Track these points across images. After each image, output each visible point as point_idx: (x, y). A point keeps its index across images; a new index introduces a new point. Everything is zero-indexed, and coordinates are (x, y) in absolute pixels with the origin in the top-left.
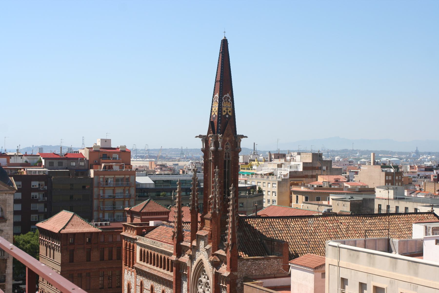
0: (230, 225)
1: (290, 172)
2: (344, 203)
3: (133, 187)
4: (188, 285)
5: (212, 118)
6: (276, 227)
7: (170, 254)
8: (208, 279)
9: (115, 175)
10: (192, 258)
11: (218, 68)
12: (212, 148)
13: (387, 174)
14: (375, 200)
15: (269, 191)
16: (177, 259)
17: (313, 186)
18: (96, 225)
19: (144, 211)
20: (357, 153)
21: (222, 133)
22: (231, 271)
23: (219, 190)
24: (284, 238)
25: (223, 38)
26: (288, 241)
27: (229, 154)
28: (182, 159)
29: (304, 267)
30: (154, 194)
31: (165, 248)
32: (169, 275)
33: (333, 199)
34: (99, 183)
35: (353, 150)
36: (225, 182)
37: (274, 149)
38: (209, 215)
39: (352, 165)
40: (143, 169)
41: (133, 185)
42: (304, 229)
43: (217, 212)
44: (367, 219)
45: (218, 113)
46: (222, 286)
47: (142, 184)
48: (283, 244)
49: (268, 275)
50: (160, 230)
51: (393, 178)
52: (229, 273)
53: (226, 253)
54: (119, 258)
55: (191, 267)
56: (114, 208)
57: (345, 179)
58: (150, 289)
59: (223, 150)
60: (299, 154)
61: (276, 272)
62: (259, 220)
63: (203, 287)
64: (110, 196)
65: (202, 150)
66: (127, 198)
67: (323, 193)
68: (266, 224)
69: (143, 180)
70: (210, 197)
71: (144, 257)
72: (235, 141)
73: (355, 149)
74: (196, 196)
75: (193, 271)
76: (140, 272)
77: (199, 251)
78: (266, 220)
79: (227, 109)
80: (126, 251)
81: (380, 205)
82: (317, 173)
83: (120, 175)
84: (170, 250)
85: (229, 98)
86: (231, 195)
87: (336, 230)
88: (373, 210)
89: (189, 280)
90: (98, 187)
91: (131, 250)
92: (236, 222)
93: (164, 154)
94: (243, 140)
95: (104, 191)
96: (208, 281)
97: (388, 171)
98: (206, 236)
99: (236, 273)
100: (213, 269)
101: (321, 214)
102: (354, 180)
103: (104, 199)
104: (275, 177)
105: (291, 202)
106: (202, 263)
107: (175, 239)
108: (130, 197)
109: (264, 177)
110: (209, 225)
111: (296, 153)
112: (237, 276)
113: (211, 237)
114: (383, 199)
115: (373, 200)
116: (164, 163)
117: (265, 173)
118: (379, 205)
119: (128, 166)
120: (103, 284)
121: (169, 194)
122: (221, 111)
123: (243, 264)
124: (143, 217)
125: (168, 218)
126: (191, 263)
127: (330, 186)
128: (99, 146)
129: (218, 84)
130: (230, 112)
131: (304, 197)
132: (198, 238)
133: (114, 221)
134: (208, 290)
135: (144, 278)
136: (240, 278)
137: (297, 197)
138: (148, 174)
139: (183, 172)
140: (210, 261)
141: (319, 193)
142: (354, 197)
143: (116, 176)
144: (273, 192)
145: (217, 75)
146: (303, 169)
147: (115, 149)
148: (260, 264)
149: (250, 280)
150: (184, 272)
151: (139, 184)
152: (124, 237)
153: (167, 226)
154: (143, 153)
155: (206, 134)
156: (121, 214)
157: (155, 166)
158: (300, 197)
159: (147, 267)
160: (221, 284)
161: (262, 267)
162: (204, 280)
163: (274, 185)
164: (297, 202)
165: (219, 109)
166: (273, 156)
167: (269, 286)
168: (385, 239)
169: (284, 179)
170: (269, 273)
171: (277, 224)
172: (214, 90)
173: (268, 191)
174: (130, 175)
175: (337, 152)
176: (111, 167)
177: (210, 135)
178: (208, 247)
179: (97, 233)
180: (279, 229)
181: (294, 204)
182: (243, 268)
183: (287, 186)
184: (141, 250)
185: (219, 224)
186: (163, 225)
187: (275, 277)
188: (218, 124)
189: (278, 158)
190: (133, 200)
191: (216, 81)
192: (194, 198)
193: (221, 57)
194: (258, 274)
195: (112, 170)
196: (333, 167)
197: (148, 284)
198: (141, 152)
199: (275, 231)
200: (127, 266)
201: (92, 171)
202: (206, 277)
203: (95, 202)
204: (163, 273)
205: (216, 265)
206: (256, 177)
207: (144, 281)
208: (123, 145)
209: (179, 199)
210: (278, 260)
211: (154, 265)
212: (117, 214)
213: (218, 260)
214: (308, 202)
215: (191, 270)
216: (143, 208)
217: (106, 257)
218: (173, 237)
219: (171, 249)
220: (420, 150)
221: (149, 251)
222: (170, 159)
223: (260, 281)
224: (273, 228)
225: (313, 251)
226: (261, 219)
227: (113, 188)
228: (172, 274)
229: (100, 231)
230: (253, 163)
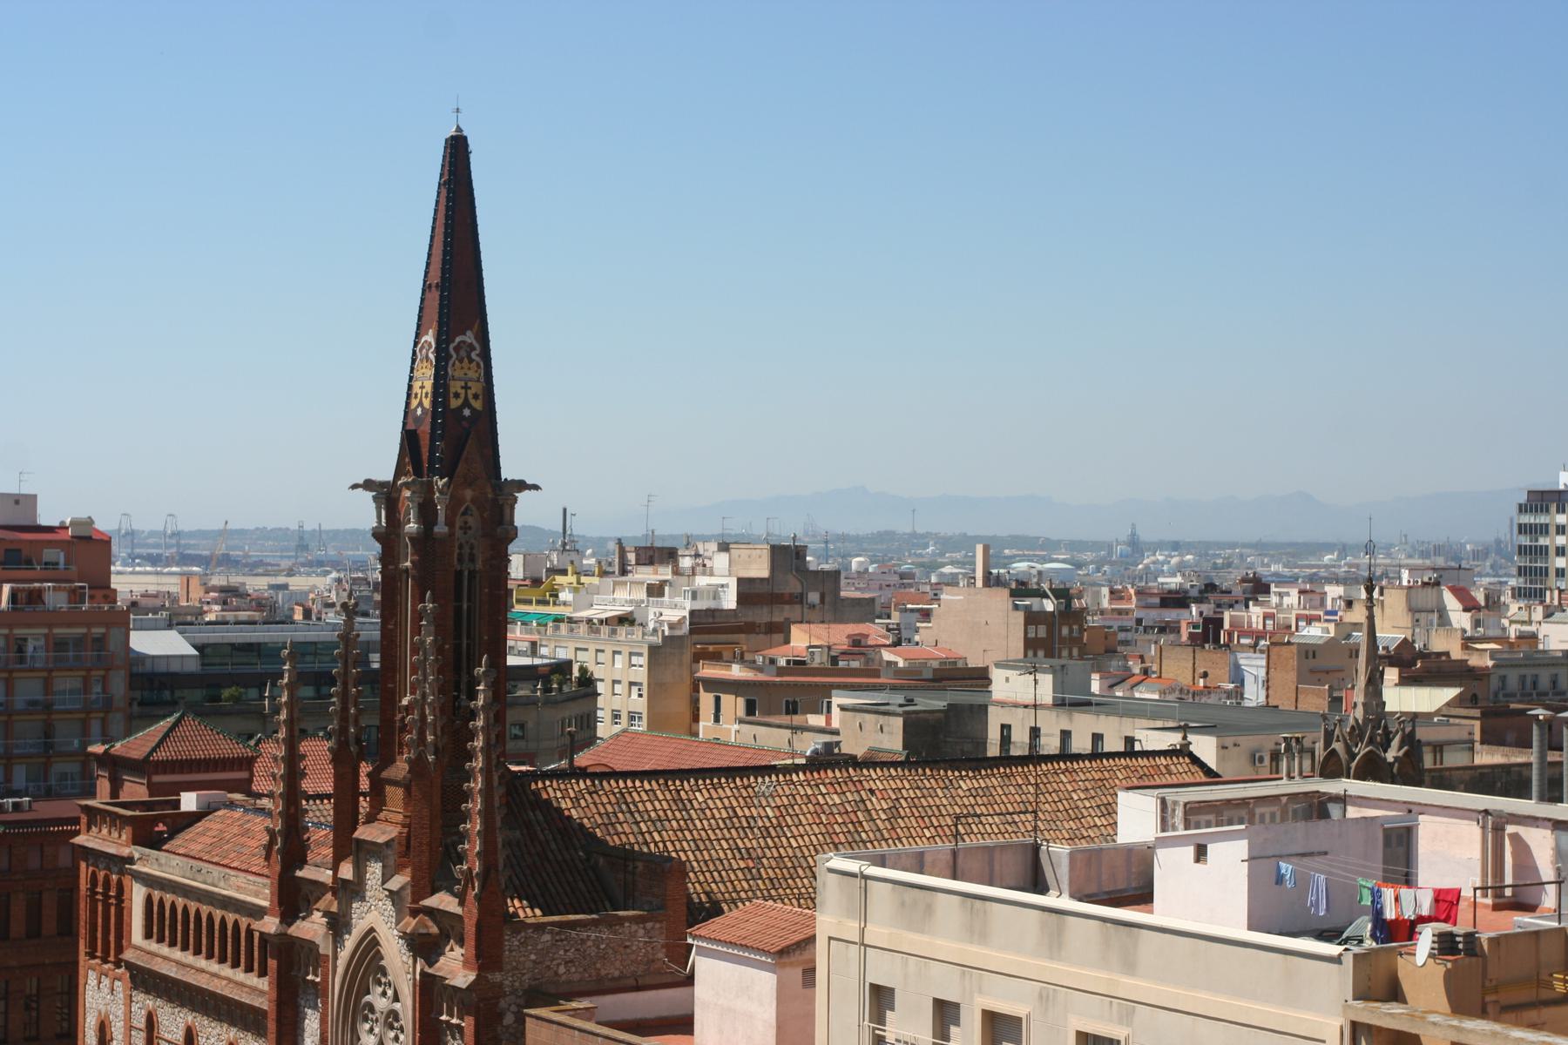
0: (476, 805)
1: (692, 613)
2: (882, 719)
4: (323, 1021)
5: (410, 420)
6: (641, 808)
7: (257, 912)
8: (396, 999)
12: (412, 526)
13: (1032, 618)
14: (991, 709)
15: (619, 682)
17: (772, 661)
19: (161, 755)
20: (926, 546)
21: (448, 472)
24: (671, 848)
25: (452, 132)
26: (684, 858)
27: (472, 548)
28: (303, 565)
29: (742, 949)
30: (197, 695)
31: (238, 889)
32: (255, 988)
33: (843, 708)
35: (914, 535)
36: (457, 649)
38: (400, 768)
39: (910, 586)
40: (158, 602)
42: (740, 813)
43: (431, 758)
45: (434, 403)
46: (447, 1022)
47: (154, 657)
48: (667, 870)
49: (614, 979)
51: (1050, 632)
52: (472, 977)
53: (462, 903)
55: (336, 958)
56: (48, 746)
59: (451, 534)
60: (724, 547)
61: (642, 968)
62: (582, 786)
63: (377, 1030)
64: (33, 703)
65: (377, 535)
67: (810, 685)
68: (605, 800)
70: (405, 702)
71: (160, 924)
72: (495, 500)
73: (920, 530)
74: (351, 701)
75: (340, 970)
76: (145, 980)
77: (363, 899)
78: (605, 783)
80: (94, 902)
81: (1006, 729)
83: (69, 625)
84: (257, 896)
88: (982, 743)
89: (325, 1003)
91: (113, 901)
94: (523, 497)
96: (397, 1006)
97: (1035, 608)
98: (388, 844)
99: (497, 977)
100: (415, 962)
101: (803, 761)
102: (917, 638)
103: (10, 715)
104: (638, 631)
105: (696, 718)
106: (375, 943)
107: (276, 858)
108: (108, 705)
109: (598, 631)
110: (401, 803)
111: (713, 546)
112: (501, 985)
113: (408, 847)
114: (1016, 705)
116: (235, 580)
117: (604, 616)
118: (1003, 726)
119: (99, 594)
122: (446, 396)
123: (523, 944)
124: (157, 779)
125: (250, 781)
127: (834, 660)
129: (435, 295)
130: (476, 397)
131: (741, 702)
133: (49, 794)
135: (159, 1002)
137: (718, 699)
138: (177, 619)
139: (307, 614)
140: (404, 936)
141: (795, 684)
142: (917, 700)
143: (56, 631)
144: (631, 684)
145: (428, 264)
146: (738, 602)
147: (50, 529)
148: (583, 941)
149: (550, 999)
150: (310, 977)
151: (142, 658)
154: (157, 546)
155: (388, 475)
157: (202, 594)
158: (727, 700)
159: (171, 960)
160: (444, 1018)
161: (593, 951)
162: (381, 1004)
163: (635, 660)
164: (717, 720)
165: (436, 386)
166: (632, 557)
168: (1024, 845)
170: (617, 973)
173: (615, 682)
174: (107, 625)
175: (857, 539)
176: (35, 597)
178: (397, 882)
181: (705, 725)
184: (149, 901)
186: (232, 805)
187: (638, 988)
188: (433, 439)
189: (651, 563)
191: (426, 288)
192: (345, 709)
194: (576, 977)
195: (40, 608)
196: (843, 594)
198: (150, 541)
199: (637, 823)
200: (94, 957)
202: (390, 992)
204: (230, 980)
205: (424, 947)
206: (572, 630)
207: (159, 1011)
208: (82, 514)
210: (649, 925)
211: (197, 952)
212: (58, 767)
213: (434, 930)
214: (757, 717)
216: (158, 746)
218: (269, 848)
219: (258, 891)
220: (1145, 535)
221: (180, 902)
222: (254, 567)
225: (773, 892)
226: (589, 782)
227: (45, 674)
228: (263, 984)
230: (559, 579)
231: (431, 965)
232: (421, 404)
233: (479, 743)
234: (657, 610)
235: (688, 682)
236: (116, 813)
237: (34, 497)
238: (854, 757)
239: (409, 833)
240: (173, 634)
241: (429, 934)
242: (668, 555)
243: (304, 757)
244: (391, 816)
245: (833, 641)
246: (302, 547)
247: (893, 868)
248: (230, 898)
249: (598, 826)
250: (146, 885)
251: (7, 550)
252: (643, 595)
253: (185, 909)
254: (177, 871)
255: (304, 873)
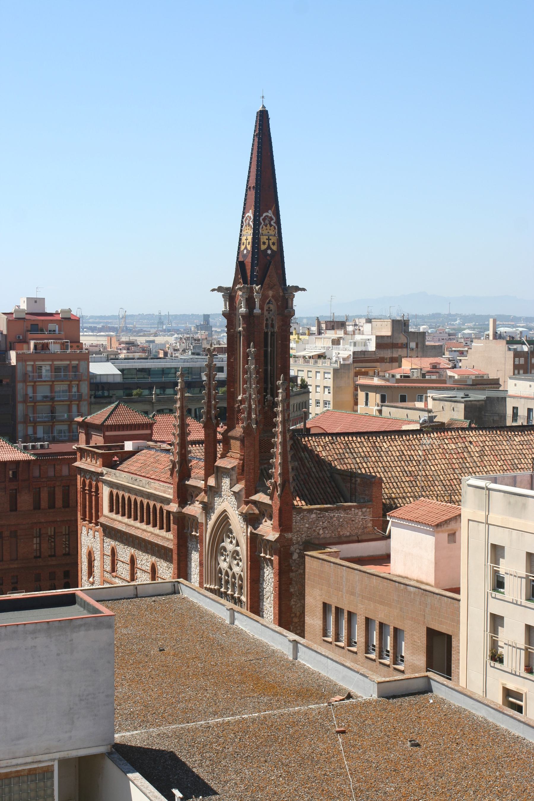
0: (278, 450)
1: (354, 353)
2: (453, 404)
3: (85, 380)
4: (201, 556)
5: (240, 256)
6: (357, 451)
7: (167, 501)
8: (238, 545)
9: (53, 360)
10: (208, 508)
11: (251, 163)
12: (243, 310)
13: (517, 354)
14: (508, 399)
15: (319, 386)
16: (180, 509)
17: (393, 376)
18: (25, 448)
20: (456, 320)
21: (261, 282)
22: (281, 531)
23: (257, 387)
24: (372, 471)
25: (260, 108)
26: (379, 476)
27: (272, 320)
28: (161, 331)
29: (416, 524)
30: (120, 393)
31: (155, 489)
32: (166, 538)
33: (434, 399)
34: (25, 374)
35: (450, 315)
36: (266, 371)
37: (326, 313)
38: (238, 431)
39: (454, 339)
40: (97, 349)
41: (84, 378)
42: (406, 454)
43: (254, 426)
44: (528, 434)
45: (253, 247)
46: (264, 557)
47: (100, 375)
48: (372, 483)
49: (347, 537)
50: (144, 458)
52: (277, 535)
53: (271, 499)
54: (69, 504)
55: (207, 524)
56: (53, 417)
57: (448, 364)
58: (129, 562)
59: (262, 314)
60: (369, 321)
61: (360, 531)
62: (327, 440)
63: (228, 560)
64: (46, 397)
65: (224, 314)
66: (75, 401)
67: (412, 388)
68: (339, 447)
69: (101, 369)
70: (240, 398)
71: (117, 505)
72: (284, 297)
73: (453, 313)
74: (212, 397)
75: (209, 530)
76: (110, 532)
77: (220, 496)
78: (338, 438)
79: (269, 239)
80: (84, 494)
81: (515, 409)
82: (399, 353)
83: (61, 360)
84: (164, 492)
85: (271, 219)
86: (280, 395)
87: (461, 454)
88: (503, 417)
89: (202, 547)
90: (25, 381)
91: (93, 494)
92: (289, 443)
93: (129, 324)
94: (298, 295)
95: (34, 388)
96: (238, 548)
97: (519, 350)
98: (233, 469)
99: (289, 535)
100: (247, 527)
101: (417, 427)
102: (460, 364)
103: (35, 403)
104: (328, 362)
105: (356, 403)
106: (226, 518)
107: (176, 475)
108: (80, 398)
109: (308, 362)
110: (239, 448)
111: (363, 321)
112: (291, 539)
113: (243, 470)
114: (521, 397)
115: (504, 399)
116: (132, 338)
117: (311, 355)
118: (514, 408)
119: (75, 345)
120: (40, 549)
121: (146, 392)
123: (302, 519)
124: (107, 433)
125: (151, 434)
126: (206, 516)
127: (424, 375)
128: (23, 310)
129: (252, 193)
131: (378, 396)
132: (220, 473)
133: (54, 440)
134: (238, 564)
135: (117, 543)
136: (298, 543)
137: (367, 395)
138: (112, 358)
139: (166, 354)
140: (241, 514)
141: (405, 387)
142: (470, 395)
143: (55, 363)
144: (325, 387)
145: (249, 177)
146: (376, 347)
147: (51, 315)
148: (331, 518)
149: (321, 546)
150: (193, 533)
151: (95, 376)
152: (80, 470)
153: (157, 450)
154: (93, 323)
155: (230, 285)
156: (65, 427)
157: (117, 345)
158: (372, 395)
159: (123, 523)
160: (262, 555)
161: (336, 523)
162: (230, 547)
163: (326, 376)
164: (367, 404)
165: (254, 239)
166: (323, 326)
167: (349, 556)
169: (344, 365)
170: (348, 534)
171: (358, 446)
172: (245, 204)
173: (317, 386)
174: (79, 360)
175: (423, 317)
176: (45, 347)
177: (238, 286)
178: (238, 488)
179: (28, 462)
180: (362, 454)
181: (361, 406)
182: (302, 526)
183: (349, 377)
184: (111, 494)
185: (257, 447)
186: (149, 448)
187: (359, 541)
188: (252, 266)
189: (333, 329)
190: (85, 403)
191: (248, 188)
192: (209, 401)
193: (256, 144)
194: (328, 536)
195: (47, 352)
196: (427, 343)
197: (124, 552)
198: (91, 320)
199: (355, 458)
200: (85, 520)
201: (13, 354)
203: (20, 408)
204: (152, 533)
205: (252, 520)
206: (296, 361)
207: (158, 563)
208: (66, 308)
209: (182, 404)
210: (364, 510)
211: (136, 519)
212: (58, 427)
213: (257, 512)
214: (386, 403)
215: (206, 529)
216: (108, 418)
217: (44, 504)
218: (172, 470)
219: (168, 491)
221: (127, 495)
222: (139, 332)
223: (334, 549)
224: (352, 453)
225: (423, 493)
226: (330, 438)
227: (51, 383)
228: (170, 535)
229: (33, 458)
231: (255, 529)
232: (246, 248)
233: (279, 419)
234: (337, 351)
235: (352, 386)
236: (94, 452)
237: (44, 299)
238: (443, 424)
239: (243, 463)
240: (109, 364)
241: (254, 514)
242: (342, 325)
243: (188, 425)
244: (233, 454)
245: (423, 366)
246: (161, 323)
247: (501, 484)
248: (151, 493)
249: (336, 460)
250: (111, 487)
251: (31, 325)
252: (330, 344)
253: (129, 498)
254: (125, 480)
255: (191, 482)
